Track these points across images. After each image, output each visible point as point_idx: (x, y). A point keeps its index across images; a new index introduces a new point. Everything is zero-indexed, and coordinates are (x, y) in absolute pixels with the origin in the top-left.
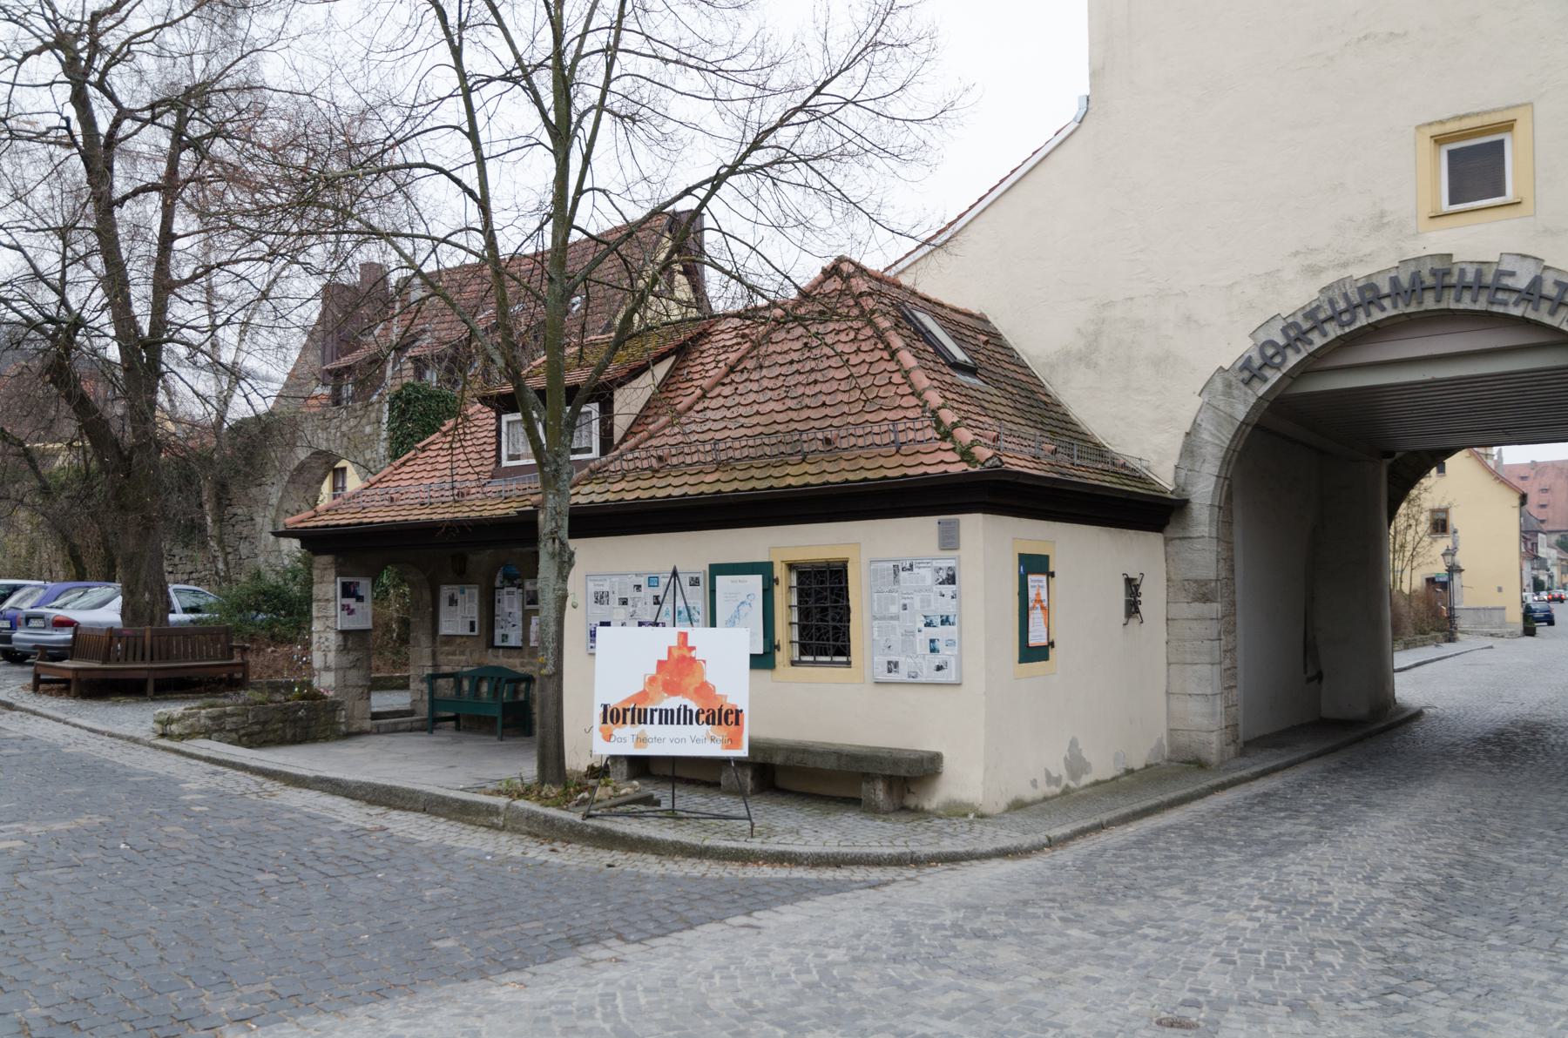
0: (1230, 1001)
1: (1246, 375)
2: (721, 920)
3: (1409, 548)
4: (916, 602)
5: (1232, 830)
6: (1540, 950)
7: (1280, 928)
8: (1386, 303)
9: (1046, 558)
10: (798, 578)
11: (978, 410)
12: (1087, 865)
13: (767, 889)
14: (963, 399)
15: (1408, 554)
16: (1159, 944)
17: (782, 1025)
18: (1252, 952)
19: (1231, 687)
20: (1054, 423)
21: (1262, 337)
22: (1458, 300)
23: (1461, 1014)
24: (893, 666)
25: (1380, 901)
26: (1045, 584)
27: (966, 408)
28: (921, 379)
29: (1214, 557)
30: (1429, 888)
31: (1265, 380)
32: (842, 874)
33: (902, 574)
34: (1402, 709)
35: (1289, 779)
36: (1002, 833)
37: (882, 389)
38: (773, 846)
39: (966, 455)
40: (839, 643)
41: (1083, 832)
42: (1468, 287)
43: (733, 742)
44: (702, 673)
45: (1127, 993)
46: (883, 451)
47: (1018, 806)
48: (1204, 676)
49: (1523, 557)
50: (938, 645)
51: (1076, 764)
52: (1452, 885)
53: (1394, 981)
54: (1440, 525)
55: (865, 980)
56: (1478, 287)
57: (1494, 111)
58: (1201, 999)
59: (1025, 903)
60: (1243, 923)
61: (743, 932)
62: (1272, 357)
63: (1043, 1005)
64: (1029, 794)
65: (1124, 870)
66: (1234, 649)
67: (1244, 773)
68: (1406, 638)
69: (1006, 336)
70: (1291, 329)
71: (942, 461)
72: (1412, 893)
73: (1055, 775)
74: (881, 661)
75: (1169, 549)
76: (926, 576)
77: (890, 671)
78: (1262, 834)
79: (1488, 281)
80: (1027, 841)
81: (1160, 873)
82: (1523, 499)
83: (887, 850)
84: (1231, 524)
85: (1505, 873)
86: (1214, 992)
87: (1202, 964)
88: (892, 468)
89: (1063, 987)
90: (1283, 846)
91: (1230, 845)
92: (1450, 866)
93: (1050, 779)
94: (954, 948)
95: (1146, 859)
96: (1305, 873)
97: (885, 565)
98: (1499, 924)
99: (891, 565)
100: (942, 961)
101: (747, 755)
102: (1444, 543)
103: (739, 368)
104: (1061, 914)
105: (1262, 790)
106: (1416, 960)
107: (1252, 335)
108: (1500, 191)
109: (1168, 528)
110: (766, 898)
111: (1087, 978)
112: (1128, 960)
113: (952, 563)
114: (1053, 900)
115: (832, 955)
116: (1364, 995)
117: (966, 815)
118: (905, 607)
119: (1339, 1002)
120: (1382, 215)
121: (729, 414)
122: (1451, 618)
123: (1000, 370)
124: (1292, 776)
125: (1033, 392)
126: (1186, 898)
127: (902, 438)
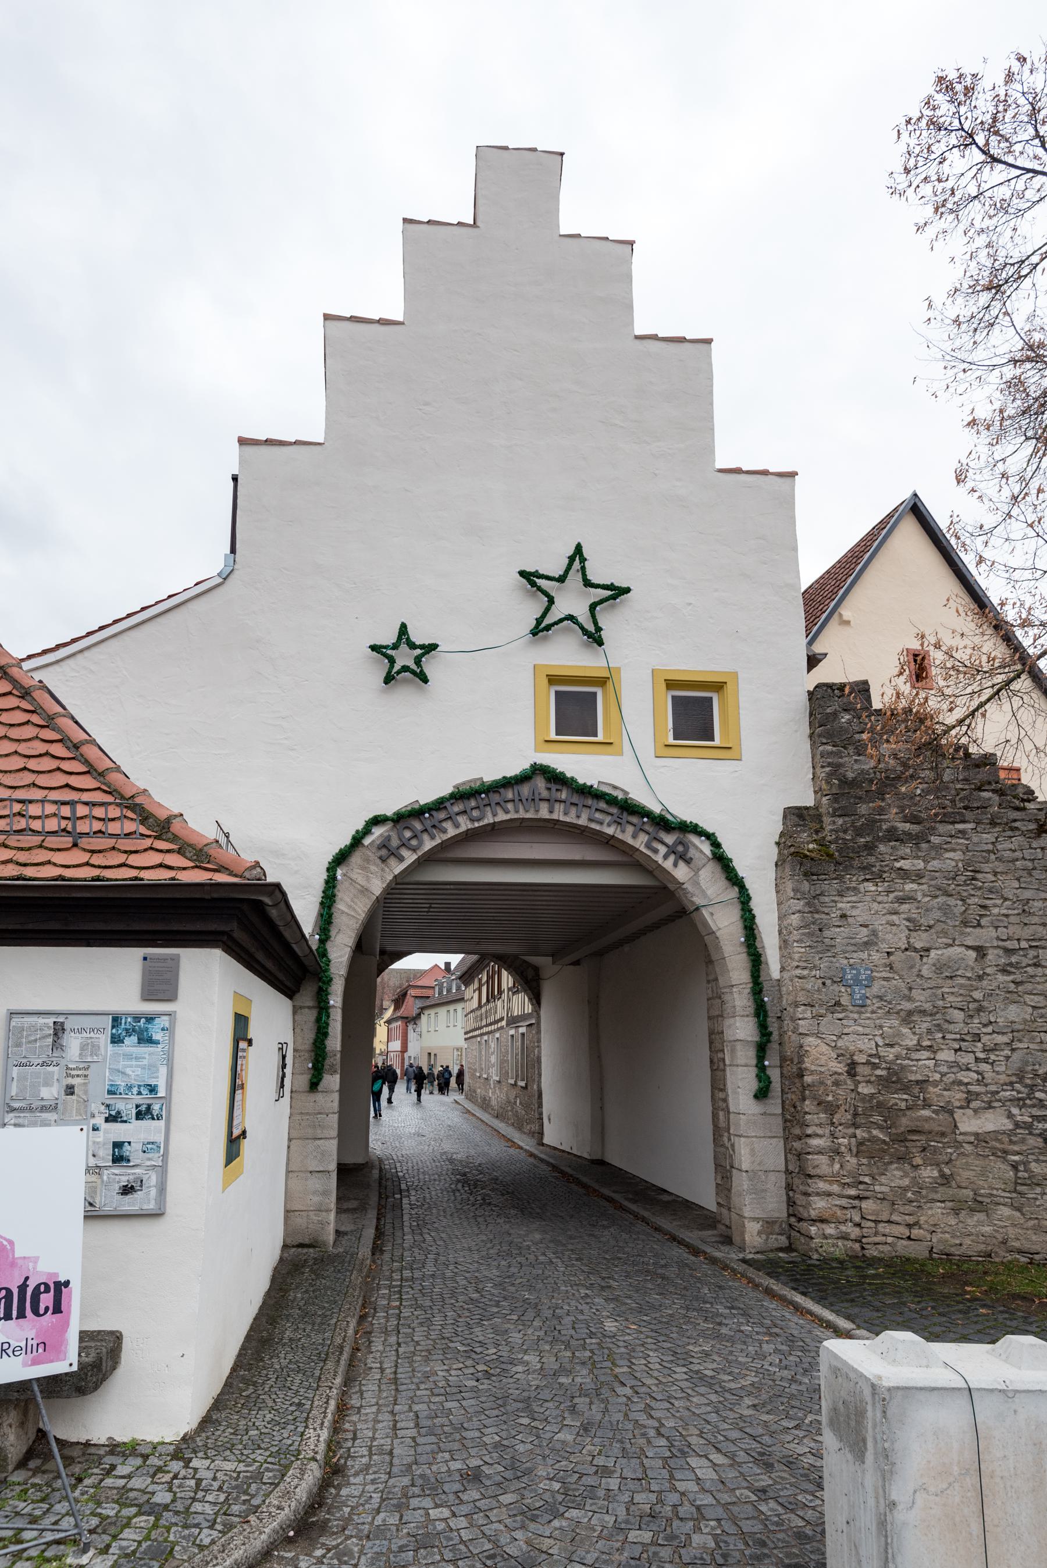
75: (296, 1018)
97: (41, 1021)
99: (50, 1021)
109: (297, 996)
118: (70, 1090)
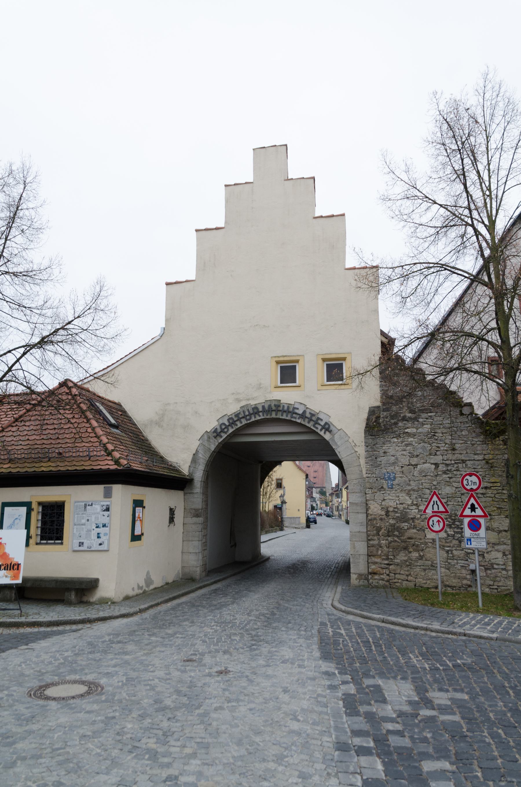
0: (206, 653)
1: (215, 434)
2: (16, 648)
3: (268, 494)
4: (93, 519)
5: (205, 602)
6: (295, 630)
7: (221, 631)
8: (261, 414)
9: (143, 501)
10: (42, 508)
11: (119, 443)
12: (154, 617)
13: (31, 636)
14: (114, 439)
15: (268, 496)
16: (182, 639)
17: (56, 676)
18: (212, 638)
19: (205, 550)
20: (146, 448)
21: (221, 422)
22: (282, 415)
23: (272, 649)
24: (81, 544)
25: (251, 620)
26: (141, 511)
27: (115, 442)
28: (99, 432)
29: (201, 500)
30: (266, 615)
31: (221, 437)
32: (61, 628)
33: (88, 507)
34: (263, 557)
35: (223, 584)
36: (122, 608)
37: (83, 434)
38: (30, 619)
39: (117, 462)
40: (58, 535)
41: (152, 607)
42: (285, 411)
43: (16, 577)
44: (4, 549)
45: (173, 654)
46: (83, 459)
47: (127, 598)
48: (196, 546)
49: (307, 497)
50: (101, 535)
51: (149, 581)
52: (273, 614)
53: (254, 642)
54: (279, 485)
55: (82, 660)
56: (288, 412)
57: (294, 356)
58: (197, 653)
59: (134, 631)
60: (209, 630)
61: (27, 651)
62: (224, 429)
63: (146, 660)
64: (131, 593)
65: (168, 618)
66: (206, 535)
67: (208, 582)
68: (266, 529)
69: (128, 412)
70: (232, 422)
71: (107, 464)
72: (261, 617)
73: (141, 585)
74: (76, 542)
76: (97, 508)
77: (80, 546)
78: (214, 603)
79: (290, 410)
80: (132, 610)
81: (181, 618)
82: (307, 476)
83: (78, 618)
84: (207, 488)
85: (289, 609)
86: (201, 651)
87: (196, 643)
88: (87, 466)
89: (152, 655)
90: (221, 606)
91: (204, 607)
92: (273, 608)
93: (139, 587)
94: (112, 647)
95: (175, 614)
96: (228, 614)
97: (81, 503)
98: (285, 624)
99: (83, 504)
100: (108, 652)
101: (21, 582)
102: (280, 492)
103: (20, 420)
104: (148, 633)
105: (214, 588)
106: (261, 636)
107: (218, 420)
108: (295, 382)
110: (32, 639)
111: (159, 651)
112: (173, 645)
113: (108, 503)
114: (144, 629)
115: (66, 654)
116: (245, 647)
117: (107, 603)
118: (88, 520)
119: (238, 650)
120: (260, 384)
121: (15, 439)
122: (282, 521)
123: (126, 426)
124: (224, 583)
125: (138, 435)
126: (190, 624)
127: (92, 454)
